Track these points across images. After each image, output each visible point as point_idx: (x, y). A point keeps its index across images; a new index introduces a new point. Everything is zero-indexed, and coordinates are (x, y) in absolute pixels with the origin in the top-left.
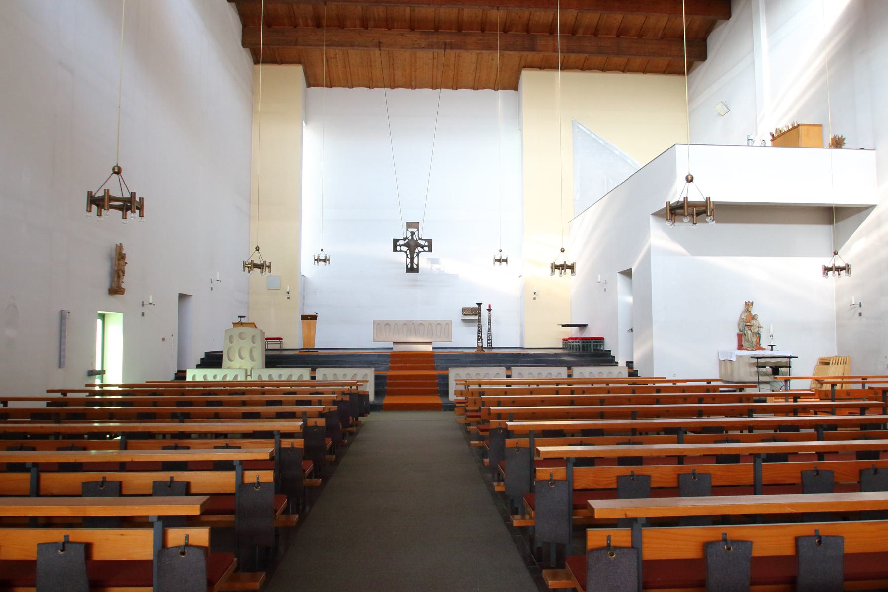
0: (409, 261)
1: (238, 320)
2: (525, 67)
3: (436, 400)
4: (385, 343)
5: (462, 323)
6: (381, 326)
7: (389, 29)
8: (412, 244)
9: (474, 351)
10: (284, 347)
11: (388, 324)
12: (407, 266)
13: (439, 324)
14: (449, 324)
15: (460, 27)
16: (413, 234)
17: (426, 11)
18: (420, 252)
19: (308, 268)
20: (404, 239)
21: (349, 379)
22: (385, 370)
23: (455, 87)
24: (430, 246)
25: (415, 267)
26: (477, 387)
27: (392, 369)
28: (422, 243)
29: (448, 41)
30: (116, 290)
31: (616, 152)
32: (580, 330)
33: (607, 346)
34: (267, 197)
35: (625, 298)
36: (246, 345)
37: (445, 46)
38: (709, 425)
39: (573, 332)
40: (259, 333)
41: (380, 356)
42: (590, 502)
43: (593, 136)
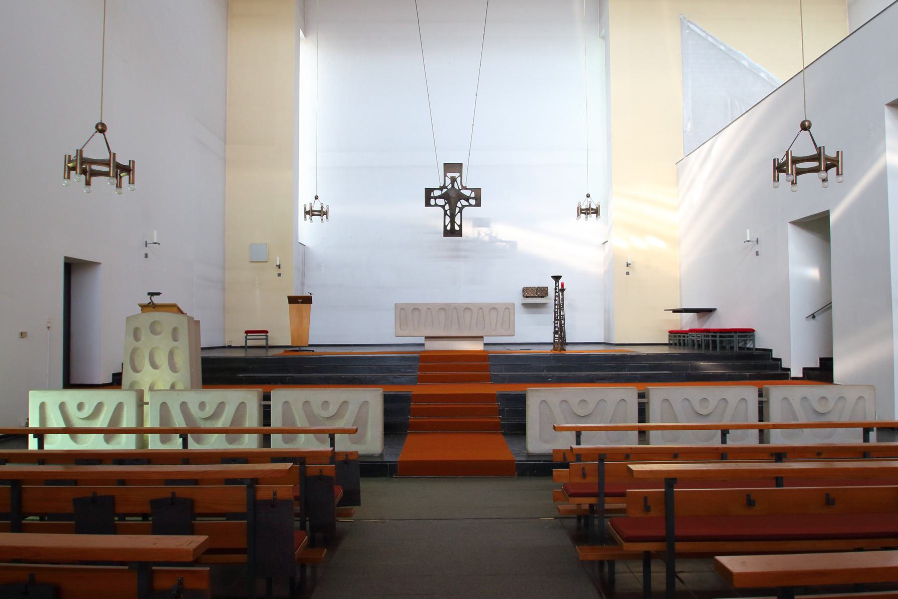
0: (448, 219)
1: (147, 300)
3: (497, 449)
4: (413, 337)
5: (523, 309)
6: (406, 313)
9: (548, 350)
10: (271, 343)
11: (416, 309)
12: (445, 227)
13: (494, 308)
14: (509, 308)
16: (453, 180)
18: (463, 206)
19: (308, 232)
20: (441, 189)
22: (412, 382)
25: (457, 228)
27: (422, 380)
28: (467, 193)
31: (745, 63)
32: (699, 318)
33: (762, 341)
34: (253, 137)
35: (802, 268)
36: (162, 344)
39: (687, 322)
40: (186, 320)
41: (402, 359)
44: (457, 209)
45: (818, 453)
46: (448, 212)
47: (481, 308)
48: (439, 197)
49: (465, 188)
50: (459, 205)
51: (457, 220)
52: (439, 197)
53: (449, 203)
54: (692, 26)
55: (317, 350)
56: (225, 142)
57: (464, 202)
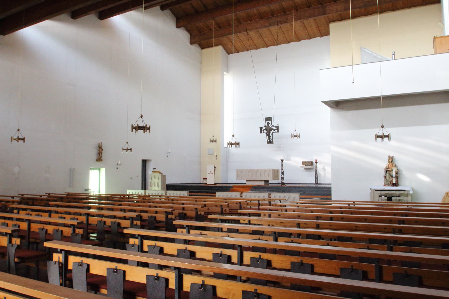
2: (331, 22)
6: (239, 172)
7: (251, 21)
12: (267, 140)
15: (273, 14)
17: (264, 8)
18: (273, 133)
20: (265, 127)
21: (257, 198)
23: (288, 42)
25: (271, 141)
26: (12, 199)
28: (274, 128)
29: (279, 20)
30: (99, 159)
34: (206, 112)
37: (278, 23)
38: (316, 234)
43: (374, 54)
47: (261, 171)
48: (265, 130)
50: (271, 132)
51: (271, 137)
52: (265, 130)
54: (366, 50)
55: (286, 185)
56: (200, 115)
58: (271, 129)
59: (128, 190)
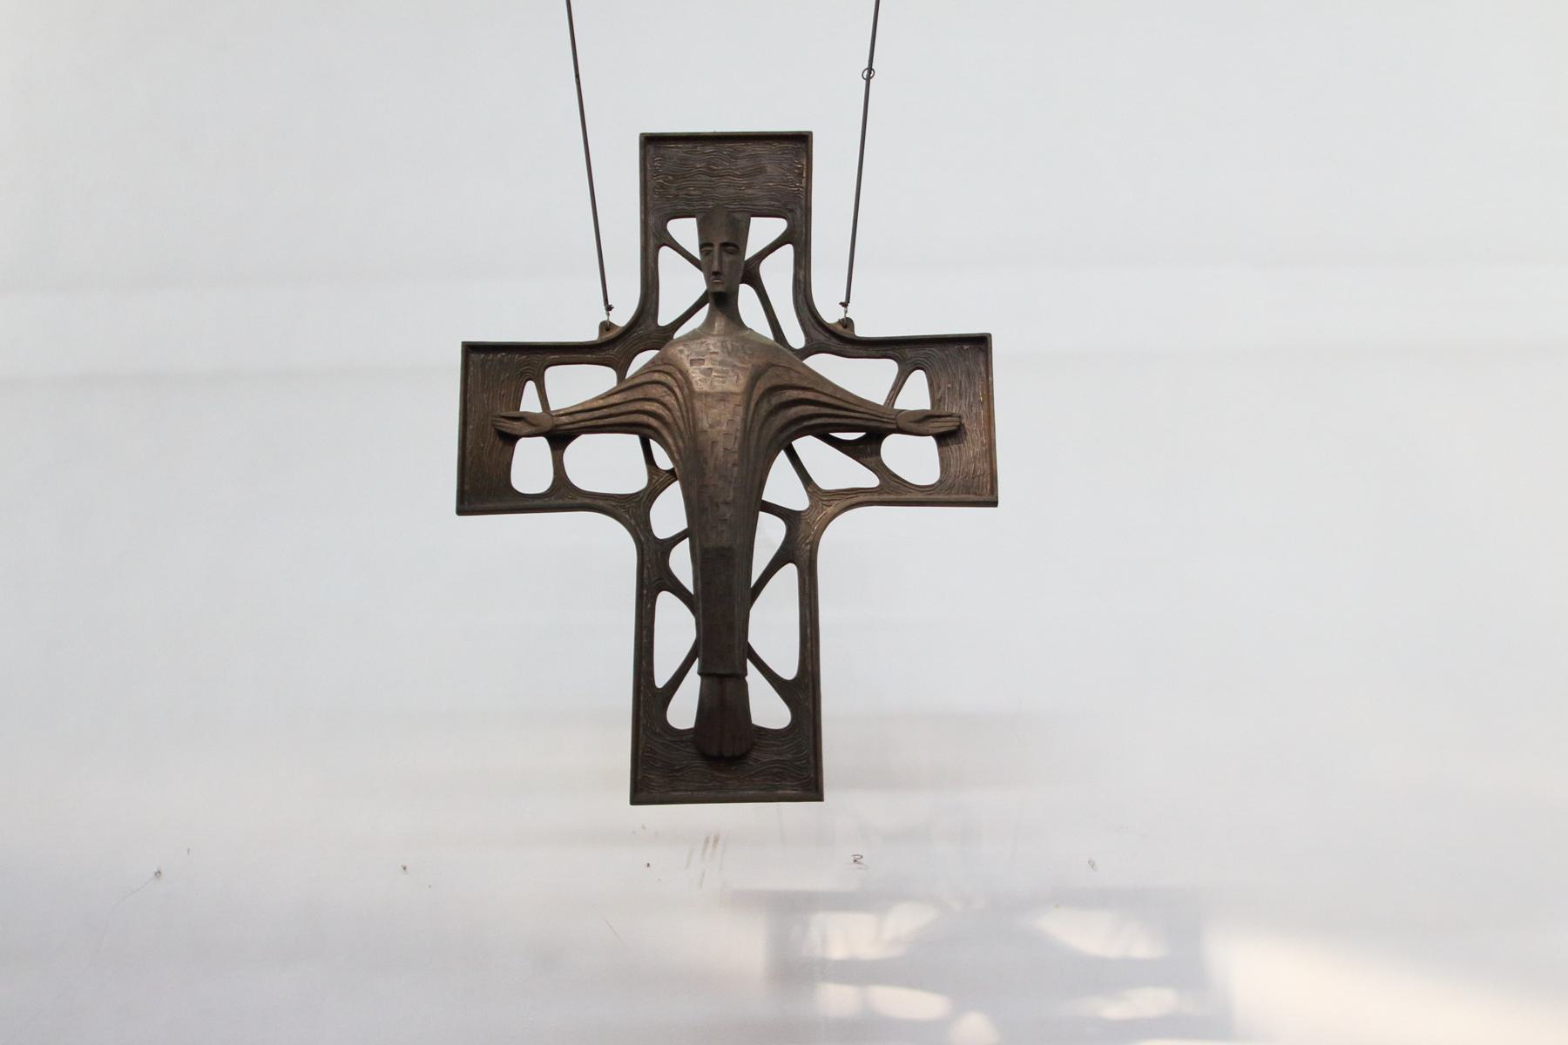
0: (677, 627)
8: (712, 375)
12: (649, 700)
20: (610, 347)
24: (963, 431)
25: (768, 710)
28: (867, 380)
42: (747, 257)
44: (770, 534)
45: (709, 789)
46: (681, 563)
49: (843, 340)
50: (782, 486)
53: (692, 472)
57: (832, 466)
58: (790, 405)
59: (755, 222)
